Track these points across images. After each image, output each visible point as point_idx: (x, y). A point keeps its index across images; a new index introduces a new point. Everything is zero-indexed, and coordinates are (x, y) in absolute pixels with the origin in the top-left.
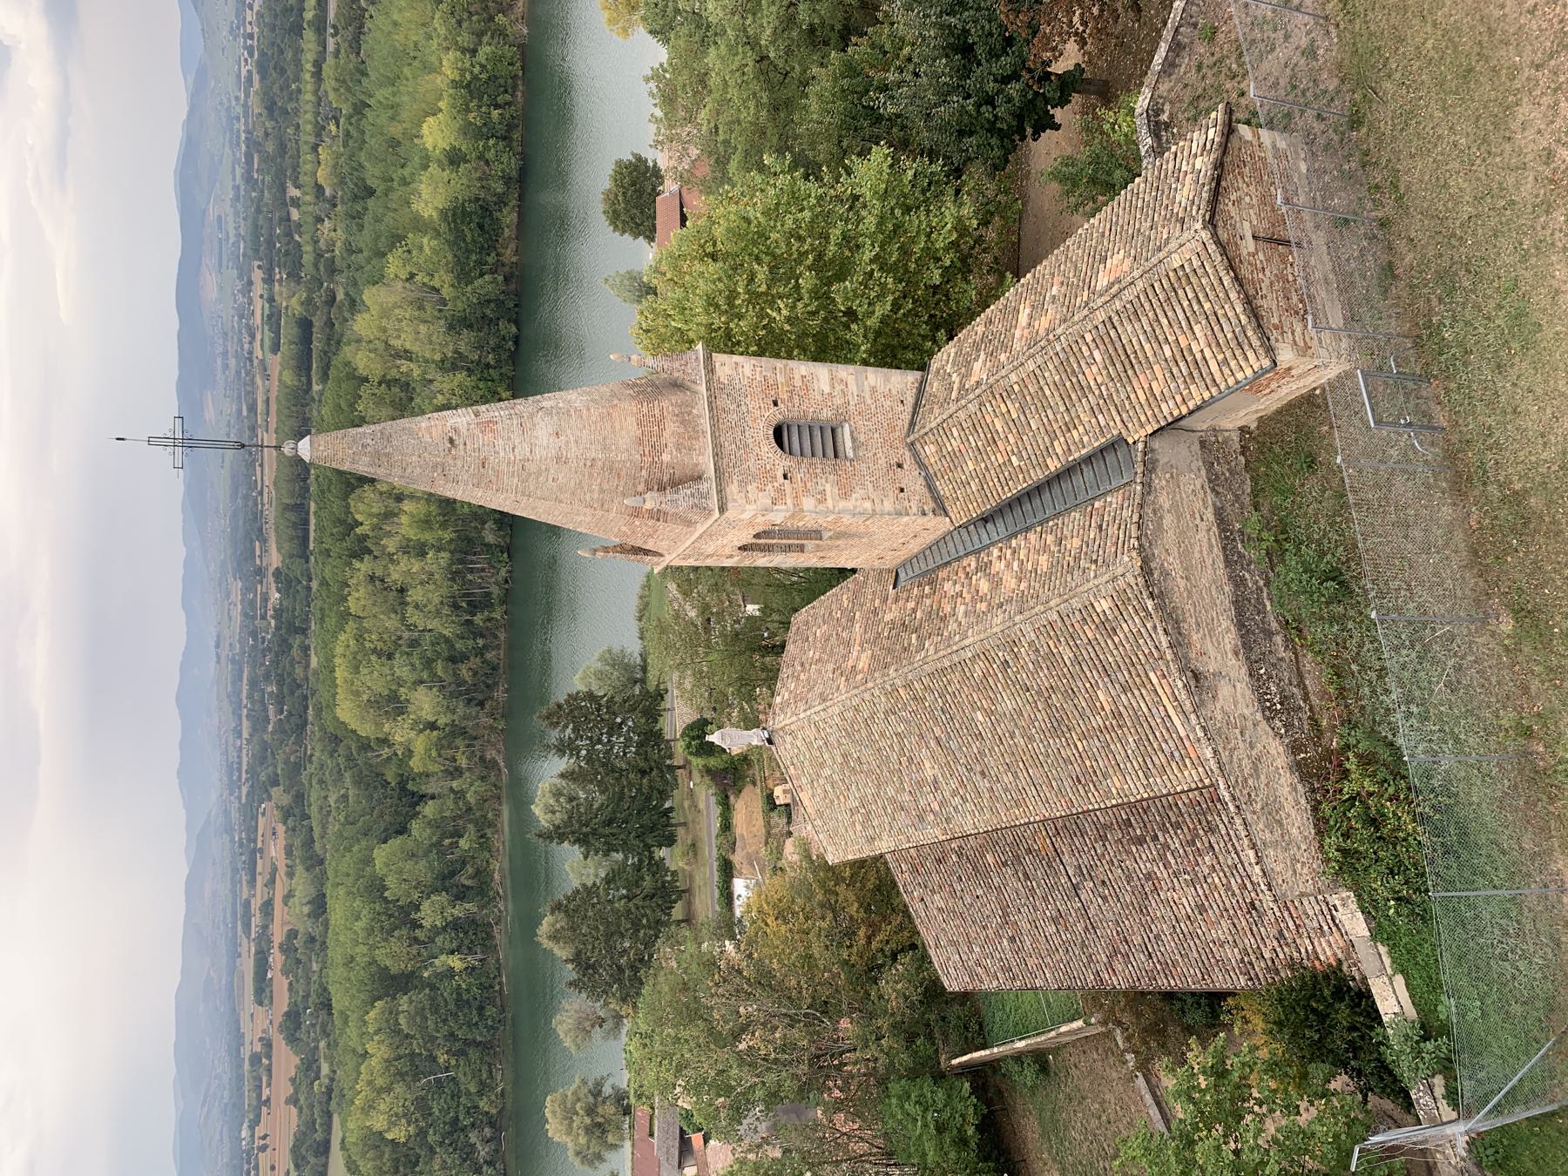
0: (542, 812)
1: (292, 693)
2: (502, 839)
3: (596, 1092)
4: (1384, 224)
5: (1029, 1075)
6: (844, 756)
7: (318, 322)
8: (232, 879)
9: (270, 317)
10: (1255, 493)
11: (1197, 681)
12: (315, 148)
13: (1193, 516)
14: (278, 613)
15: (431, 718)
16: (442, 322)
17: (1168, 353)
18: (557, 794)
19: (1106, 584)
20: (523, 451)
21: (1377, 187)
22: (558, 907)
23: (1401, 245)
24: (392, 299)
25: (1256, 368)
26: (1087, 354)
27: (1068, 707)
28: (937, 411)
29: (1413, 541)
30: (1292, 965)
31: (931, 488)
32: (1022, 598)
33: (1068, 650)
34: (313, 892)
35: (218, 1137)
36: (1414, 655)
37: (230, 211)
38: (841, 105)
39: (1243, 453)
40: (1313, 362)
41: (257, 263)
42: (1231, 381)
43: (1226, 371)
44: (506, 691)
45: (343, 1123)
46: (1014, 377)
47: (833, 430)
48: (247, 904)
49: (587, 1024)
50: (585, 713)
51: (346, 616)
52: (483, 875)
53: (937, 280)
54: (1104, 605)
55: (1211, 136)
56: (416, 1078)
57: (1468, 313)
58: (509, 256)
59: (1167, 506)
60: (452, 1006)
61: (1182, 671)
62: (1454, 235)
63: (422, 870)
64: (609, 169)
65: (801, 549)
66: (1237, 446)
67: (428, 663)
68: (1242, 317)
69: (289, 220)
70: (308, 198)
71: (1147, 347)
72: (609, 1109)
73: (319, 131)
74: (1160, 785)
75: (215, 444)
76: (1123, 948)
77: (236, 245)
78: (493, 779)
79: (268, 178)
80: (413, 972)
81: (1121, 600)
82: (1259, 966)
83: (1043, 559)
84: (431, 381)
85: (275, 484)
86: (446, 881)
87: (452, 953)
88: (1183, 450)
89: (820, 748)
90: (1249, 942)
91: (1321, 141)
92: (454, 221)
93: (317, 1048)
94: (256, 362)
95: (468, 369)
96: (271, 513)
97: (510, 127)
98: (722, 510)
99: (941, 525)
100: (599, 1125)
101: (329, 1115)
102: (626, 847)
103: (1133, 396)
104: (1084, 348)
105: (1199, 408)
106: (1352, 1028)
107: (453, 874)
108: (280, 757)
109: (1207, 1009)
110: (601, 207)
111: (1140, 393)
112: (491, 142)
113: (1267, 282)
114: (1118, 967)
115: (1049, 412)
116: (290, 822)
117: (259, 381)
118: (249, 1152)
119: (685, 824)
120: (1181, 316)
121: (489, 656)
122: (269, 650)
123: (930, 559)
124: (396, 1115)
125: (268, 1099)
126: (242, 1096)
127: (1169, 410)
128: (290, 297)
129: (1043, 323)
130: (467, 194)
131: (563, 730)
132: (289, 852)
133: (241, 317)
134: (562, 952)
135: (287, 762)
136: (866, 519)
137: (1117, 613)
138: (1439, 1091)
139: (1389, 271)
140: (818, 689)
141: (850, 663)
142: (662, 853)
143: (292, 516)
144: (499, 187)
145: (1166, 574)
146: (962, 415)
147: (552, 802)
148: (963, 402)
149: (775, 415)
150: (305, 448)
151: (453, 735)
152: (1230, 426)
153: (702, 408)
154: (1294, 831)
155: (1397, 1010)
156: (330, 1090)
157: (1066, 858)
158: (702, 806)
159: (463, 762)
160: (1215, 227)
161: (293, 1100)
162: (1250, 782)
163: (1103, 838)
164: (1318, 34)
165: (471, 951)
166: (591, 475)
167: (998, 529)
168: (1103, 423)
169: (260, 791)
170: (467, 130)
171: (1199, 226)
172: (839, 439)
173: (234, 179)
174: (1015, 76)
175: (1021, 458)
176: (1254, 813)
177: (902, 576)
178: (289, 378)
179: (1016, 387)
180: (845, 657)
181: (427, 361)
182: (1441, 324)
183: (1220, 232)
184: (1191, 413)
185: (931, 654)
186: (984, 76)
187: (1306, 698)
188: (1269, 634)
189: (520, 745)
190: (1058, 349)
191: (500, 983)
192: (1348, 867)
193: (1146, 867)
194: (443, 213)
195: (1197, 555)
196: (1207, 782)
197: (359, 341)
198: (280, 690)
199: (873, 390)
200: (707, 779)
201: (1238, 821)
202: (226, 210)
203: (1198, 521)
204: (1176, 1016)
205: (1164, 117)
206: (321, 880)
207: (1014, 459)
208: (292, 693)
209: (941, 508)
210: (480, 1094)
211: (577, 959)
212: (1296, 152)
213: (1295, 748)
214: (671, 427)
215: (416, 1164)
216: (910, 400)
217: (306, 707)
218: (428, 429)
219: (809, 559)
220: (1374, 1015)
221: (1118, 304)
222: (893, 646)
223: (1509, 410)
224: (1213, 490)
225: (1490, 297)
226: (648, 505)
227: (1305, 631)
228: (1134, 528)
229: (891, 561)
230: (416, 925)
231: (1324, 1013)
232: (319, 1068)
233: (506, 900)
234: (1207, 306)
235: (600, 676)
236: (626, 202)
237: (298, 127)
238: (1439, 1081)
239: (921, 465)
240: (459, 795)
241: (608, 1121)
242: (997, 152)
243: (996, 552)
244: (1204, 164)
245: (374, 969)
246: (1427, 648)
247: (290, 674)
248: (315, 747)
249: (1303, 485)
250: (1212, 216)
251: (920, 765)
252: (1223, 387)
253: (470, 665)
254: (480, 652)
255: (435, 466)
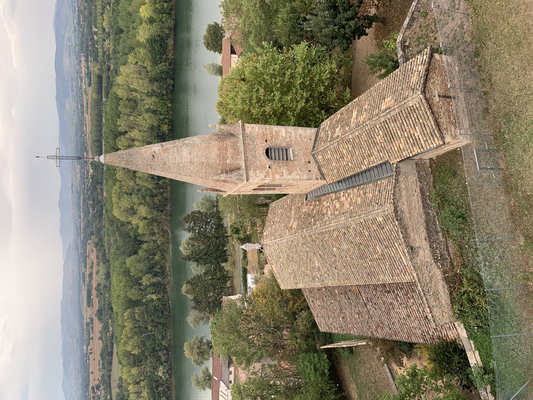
0: (184, 249)
1: (98, 204)
2: (169, 256)
3: (201, 341)
4: (485, 93)
5: (347, 353)
6: (288, 256)
7: (104, 76)
8: (79, 266)
9: (87, 74)
10: (434, 182)
11: (412, 250)
12: (102, 14)
13: (412, 190)
14: (93, 177)
15: (145, 216)
16: (147, 79)
17: (406, 135)
18: (188, 244)
19: (382, 212)
20: (178, 159)
21: (484, 80)
22: (188, 282)
23: (491, 102)
24: (130, 71)
25: (438, 143)
26: (377, 132)
27: (366, 250)
28: (323, 144)
29: (490, 206)
30: (439, 338)
31: (320, 170)
32: (351, 212)
33: (367, 232)
34: (106, 271)
35: (76, 349)
36: (488, 245)
37: (73, 35)
38: (289, 23)
39: (430, 168)
40: (457, 140)
41: (82, 54)
42: (428, 147)
43: (427, 144)
44: (170, 207)
45: (117, 348)
46: (350, 136)
47: (286, 150)
48: (84, 274)
49: (198, 320)
50: (197, 218)
51: (116, 180)
52: (163, 268)
53: (322, 90)
54: (380, 219)
55: (425, 58)
56: (141, 334)
57: (515, 130)
58: (170, 56)
59: (403, 187)
60: (153, 311)
61: (407, 246)
62: (511, 101)
63: (142, 266)
64: (206, 27)
65: (274, 189)
66: (428, 165)
67: (144, 197)
68: (434, 126)
69: (93, 39)
70: (100, 32)
71: (399, 132)
72: (205, 347)
73: (103, 8)
74: (397, 280)
75: (68, 158)
76: (381, 325)
77: (75, 47)
78: (166, 236)
79: (86, 24)
80: (140, 300)
81: (386, 218)
82: (428, 337)
83: (359, 199)
84: (144, 100)
85: (90, 133)
86: (150, 270)
87: (153, 294)
88: (410, 167)
89: (279, 252)
90: (425, 328)
91: (464, 59)
92: (151, 43)
93: (108, 322)
94: (83, 90)
95: (157, 96)
96: (89, 142)
97: (171, 10)
98: (247, 180)
99: (324, 182)
100: (202, 352)
101: (113, 344)
102: (211, 262)
103: (393, 148)
104: (376, 130)
105: (416, 155)
106: (459, 363)
107: (153, 268)
108: (94, 225)
109: (409, 348)
110: (203, 41)
111: (395, 147)
112: (164, 15)
113: (443, 112)
114: (379, 331)
115: (363, 150)
116: (98, 247)
117: (84, 96)
118: (86, 354)
119: (231, 255)
120: (411, 123)
121: (164, 195)
122: (90, 189)
123: (318, 192)
124: (134, 346)
125: (92, 337)
126: (83, 336)
127: (405, 154)
128: (94, 68)
129: (361, 119)
130: (156, 34)
131: (190, 224)
132: (97, 257)
133: (78, 73)
134: (190, 297)
135: (96, 227)
136: (295, 180)
137: (384, 222)
138: (489, 390)
139: (486, 111)
140: (279, 232)
141: (290, 225)
142: (223, 264)
143: (97, 144)
144: (167, 31)
145: (402, 212)
146: (332, 147)
147: (186, 246)
148: (332, 143)
149: (266, 145)
150: (102, 159)
151: (152, 221)
152: (426, 158)
153: (241, 144)
154: (443, 301)
155: (476, 363)
156: (112, 336)
157: (363, 294)
158: (237, 249)
159: (156, 230)
160: (425, 93)
161: (100, 338)
162: (429, 285)
163: (376, 290)
164: (464, 20)
165: (159, 293)
166: (202, 168)
167: (343, 186)
168: (382, 156)
169: (88, 236)
170: (155, 10)
171: (419, 93)
172: (288, 154)
173: (74, 24)
174: (352, 18)
175: (352, 164)
176: (430, 295)
177: (309, 196)
178: (94, 96)
179: (351, 140)
180: (289, 222)
181: (142, 93)
182: (504, 132)
183: (427, 94)
184: (413, 156)
185: (318, 227)
186: (341, 17)
187: (449, 255)
188: (437, 232)
189: (175, 225)
190: (367, 129)
191: (169, 304)
192: (461, 315)
193: (390, 301)
194: (147, 40)
195: (413, 205)
196: (413, 281)
197: (119, 85)
198: (94, 203)
199: (300, 135)
200: (239, 241)
201: (424, 298)
202: (71, 35)
203: (414, 192)
204: (397, 349)
205: (407, 44)
206: (108, 268)
207: (350, 164)
208: (98, 204)
209: (323, 177)
210: (162, 339)
211: (195, 299)
212: (455, 63)
213: (444, 272)
214: (230, 151)
215: (141, 361)
216: (313, 139)
217: (102, 209)
218: (145, 152)
219: (277, 192)
220: (468, 364)
221: (389, 116)
222: (306, 221)
223: (527, 166)
224: (420, 181)
225: (523, 125)
226: (222, 179)
227: (450, 232)
228: (392, 195)
229: (305, 191)
230: (140, 284)
231: (449, 356)
232: (109, 328)
233: (171, 276)
234: (421, 121)
235: (202, 204)
236: (212, 40)
237: (96, 6)
238: (489, 387)
239: (317, 162)
240: (155, 241)
241: (205, 351)
242: (345, 45)
243: (342, 194)
244: (422, 69)
245: (126, 299)
246: (493, 243)
247: (97, 198)
248: (106, 223)
249: (451, 181)
250: (424, 89)
251: (314, 262)
252: (425, 149)
253: (158, 198)
254: (161, 194)
255: (148, 165)
